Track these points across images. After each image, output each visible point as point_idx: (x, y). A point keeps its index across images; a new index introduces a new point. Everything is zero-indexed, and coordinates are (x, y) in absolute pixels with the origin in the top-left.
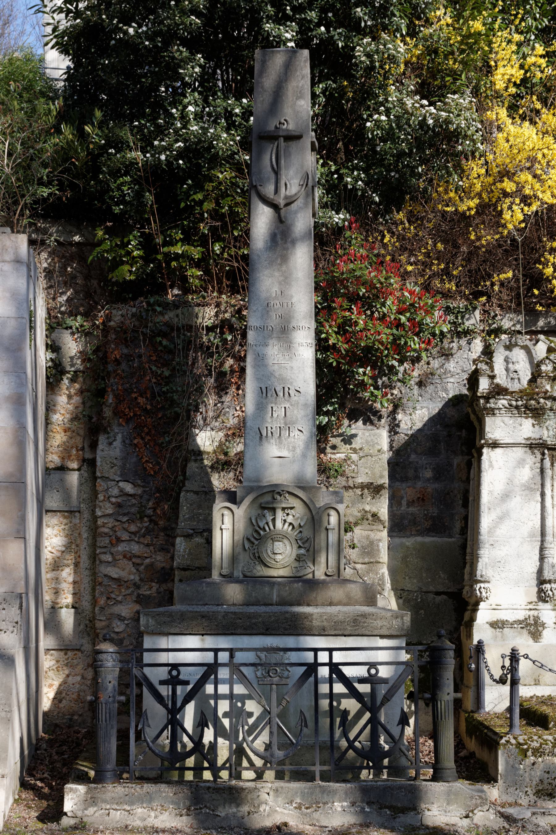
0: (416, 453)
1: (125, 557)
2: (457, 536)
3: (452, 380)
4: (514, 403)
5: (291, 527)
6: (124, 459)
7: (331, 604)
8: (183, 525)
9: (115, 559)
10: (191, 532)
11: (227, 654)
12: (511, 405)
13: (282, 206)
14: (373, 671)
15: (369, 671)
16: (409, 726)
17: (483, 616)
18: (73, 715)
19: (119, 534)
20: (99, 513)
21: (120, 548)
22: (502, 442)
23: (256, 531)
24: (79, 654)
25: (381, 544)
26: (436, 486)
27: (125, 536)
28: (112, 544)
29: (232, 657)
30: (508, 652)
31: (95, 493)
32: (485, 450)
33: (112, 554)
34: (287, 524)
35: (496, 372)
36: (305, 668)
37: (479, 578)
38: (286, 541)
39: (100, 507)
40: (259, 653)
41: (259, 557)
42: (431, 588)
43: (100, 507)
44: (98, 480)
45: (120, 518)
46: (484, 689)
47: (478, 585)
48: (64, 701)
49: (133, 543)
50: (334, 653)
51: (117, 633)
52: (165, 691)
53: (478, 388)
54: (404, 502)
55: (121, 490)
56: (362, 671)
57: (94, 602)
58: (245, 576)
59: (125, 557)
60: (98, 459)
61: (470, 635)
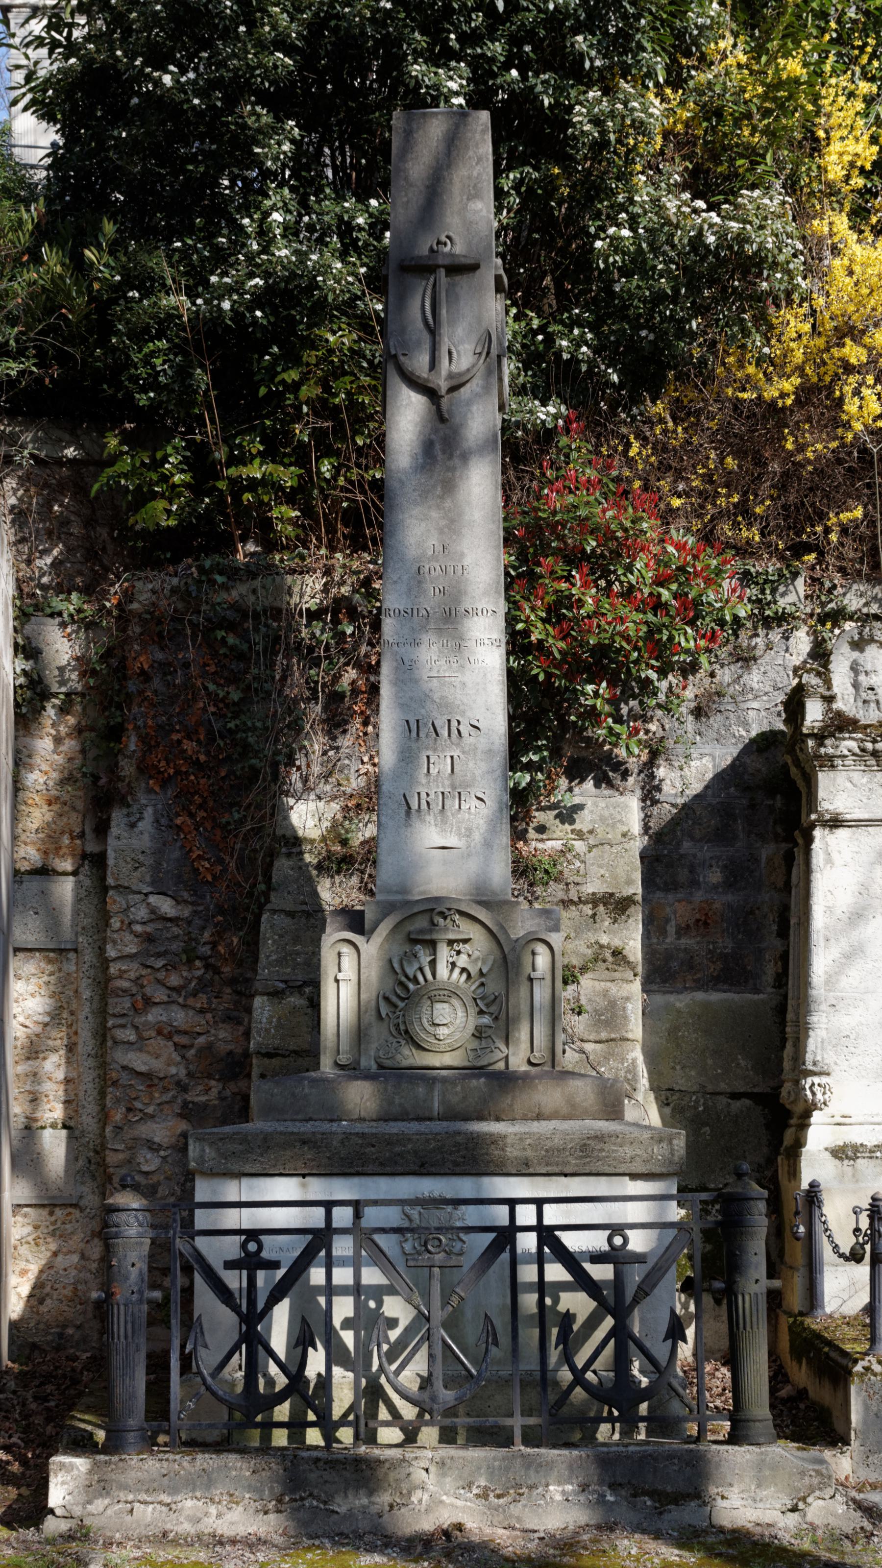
0: (692, 838)
1: (159, 1033)
2: (770, 990)
3: (755, 705)
4: (869, 746)
5: (464, 976)
6: (158, 853)
7: (539, 1117)
8: (267, 971)
9: (141, 1038)
10: (282, 985)
11: (349, 1211)
12: (863, 750)
13: (443, 391)
14: (618, 1241)
15: (610, 1240)
16: (685, 1341)
17: (819, 1136)
18: (65, 1327)
19: (148, 991)
20: (111, 953)
21: (150, 1017)
22: (848, 817)
23: (401, 984)
24: (76, 1213)
25: (629, 1006)
26: (730, 898)
27: (160, 995)
28: (136, 1010)
29: (357, 1215)
30: (865, 1203)
31: (104, 916)
32: (818, 833)
33: (136, 1028)
34: (457, 971)
35: (836, 689)
36: (493, 1235)
37: (810, 1067)
38: (455, 1001)
39: (114, 942)
40: (407, 1209)
41: (407, 1032)
42: (723, 1087)
43: (114, 942)
44: (111, 893)
45: (151, 961)
46: (821, 1272)
47: (809, 1080)
48: (48, 1301)
49: (175, 1007)
50: (547, 1207)
51: (147, 1173)
52: (234, 1280)
53: (803, 719)
54: (671, 929)
55: (153, 911)
56: (597, 1241)
57: (104, 1117)
58: (381, 1067)
59: (159, 1033)
60: (111, 854)
61: (794, 1172)
